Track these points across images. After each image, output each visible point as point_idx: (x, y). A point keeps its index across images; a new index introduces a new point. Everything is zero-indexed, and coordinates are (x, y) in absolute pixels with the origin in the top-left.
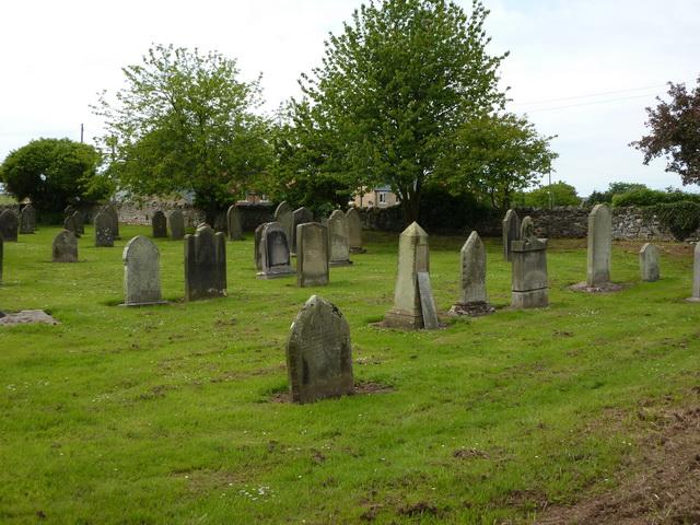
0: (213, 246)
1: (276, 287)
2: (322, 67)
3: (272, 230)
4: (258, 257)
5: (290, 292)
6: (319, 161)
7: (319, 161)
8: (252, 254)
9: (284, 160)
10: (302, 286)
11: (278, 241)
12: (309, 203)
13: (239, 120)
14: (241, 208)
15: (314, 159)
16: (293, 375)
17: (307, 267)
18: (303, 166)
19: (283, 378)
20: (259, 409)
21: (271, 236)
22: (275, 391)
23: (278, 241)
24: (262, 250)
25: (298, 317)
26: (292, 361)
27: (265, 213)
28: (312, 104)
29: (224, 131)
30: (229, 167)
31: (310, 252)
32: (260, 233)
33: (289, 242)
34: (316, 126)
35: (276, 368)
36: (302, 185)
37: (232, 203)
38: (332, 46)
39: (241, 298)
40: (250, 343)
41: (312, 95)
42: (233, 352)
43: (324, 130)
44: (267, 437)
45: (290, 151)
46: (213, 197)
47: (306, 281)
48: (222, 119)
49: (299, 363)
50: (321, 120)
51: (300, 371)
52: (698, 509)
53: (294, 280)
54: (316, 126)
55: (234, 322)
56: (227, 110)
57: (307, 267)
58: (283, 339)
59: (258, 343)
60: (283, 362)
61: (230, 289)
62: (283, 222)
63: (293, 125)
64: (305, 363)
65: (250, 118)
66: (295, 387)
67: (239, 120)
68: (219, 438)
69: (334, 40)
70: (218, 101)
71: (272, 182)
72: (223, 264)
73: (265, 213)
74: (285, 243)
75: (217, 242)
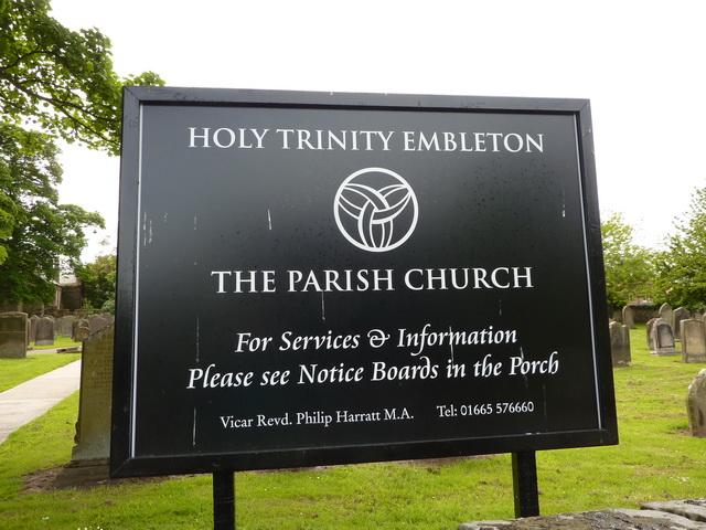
0: (620, 334)
1: (666, 362)
2: (690, 211)
3: (661, 323)
4: (650, 341)
5: (678, 366)
6: (692, 275)
7: (692, 275)
8: (645, 339)
9: (663, 275)
10: (687, 362)
11: (665, 330)
12: (685, 303)
13: (627, 249)
14: (632, 307)
15: (687, 274)
16: (692, 418)
17: (690, 349)
18: (678, 278)
19: (686, 421)
20: (670, 437)
21: (659, 328)
22: (679, 428)
23: (665, 330)
24: (653, 336)
25: (693, 382)
26: (691, 410)
27: (652, 310)
28: (683, 236)
29: (617, 258)
30: (622, 280)
31: (692, 339)
32: (651, 326)
33: (675, 331)
34: (687, 250)
35: (680, 415)
36: (680, 293)
37: (625, 304)
38: (698, 197)
39: (642, 368)
40: (653, 397)
41: (684, 230)
42: (644, 402)
43: (694, 254)
44: (681, 454)
45: (668, 269)
46: (612, 300)
47: (689, 359)
48: (614, 250)
49: (697, 412)
50: (692, 247)
51: (697, 417)
52: (704, 281)
53: (680, 358)
54: (687, 250)
55: (640, 384)
56: (618, 244)
57: (690, 349)
58: (683, 396)
59: (661, 398)
60: (685, 412)
61: (633, 362)
62: (665, 317)
63: (670, 251)
64: (700, 412)
65: (635, 248)
66: (693, 427)
67: (627, 249)
68: (649, 450)
69: (698, 192)
70: (612, 238)
71: (655, 289)
72: (628, 347)
73: (652, 310)
74: (670, 332)
75: (624, 332)
